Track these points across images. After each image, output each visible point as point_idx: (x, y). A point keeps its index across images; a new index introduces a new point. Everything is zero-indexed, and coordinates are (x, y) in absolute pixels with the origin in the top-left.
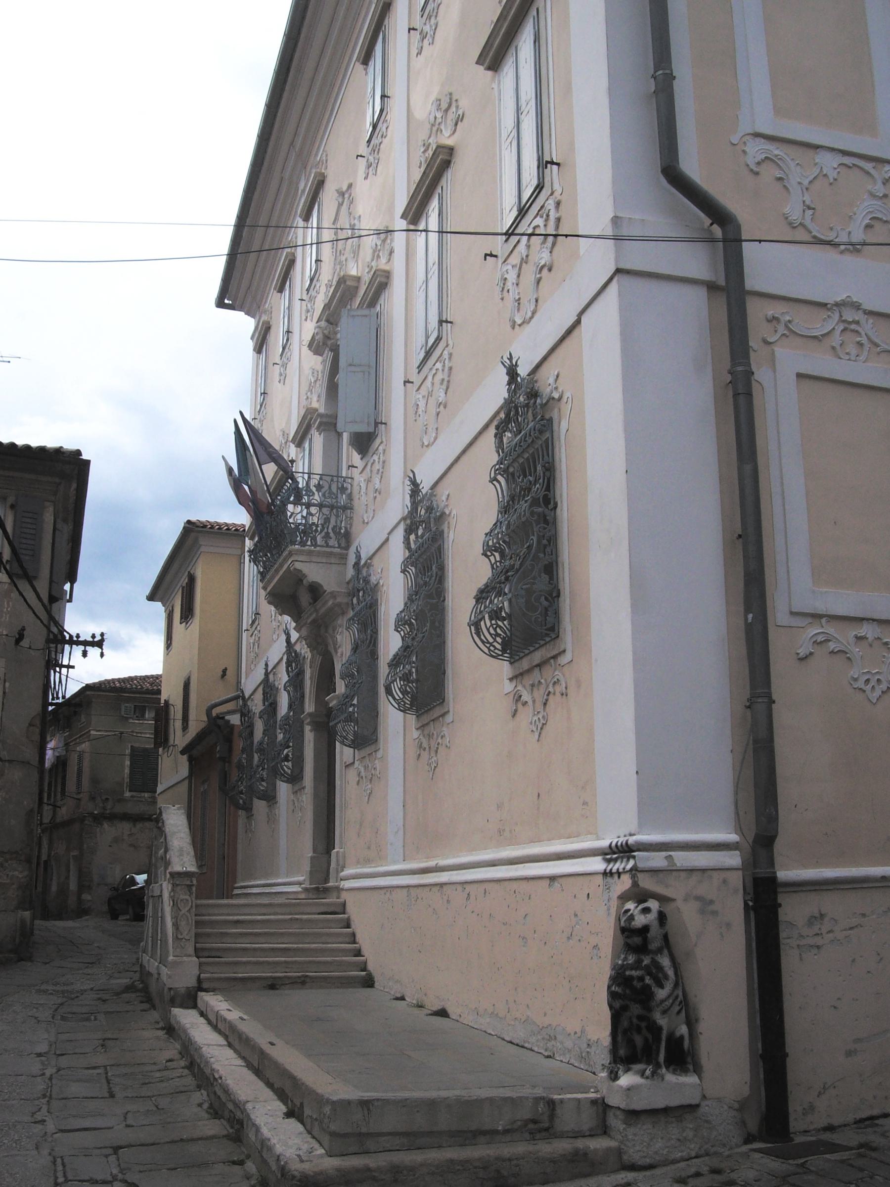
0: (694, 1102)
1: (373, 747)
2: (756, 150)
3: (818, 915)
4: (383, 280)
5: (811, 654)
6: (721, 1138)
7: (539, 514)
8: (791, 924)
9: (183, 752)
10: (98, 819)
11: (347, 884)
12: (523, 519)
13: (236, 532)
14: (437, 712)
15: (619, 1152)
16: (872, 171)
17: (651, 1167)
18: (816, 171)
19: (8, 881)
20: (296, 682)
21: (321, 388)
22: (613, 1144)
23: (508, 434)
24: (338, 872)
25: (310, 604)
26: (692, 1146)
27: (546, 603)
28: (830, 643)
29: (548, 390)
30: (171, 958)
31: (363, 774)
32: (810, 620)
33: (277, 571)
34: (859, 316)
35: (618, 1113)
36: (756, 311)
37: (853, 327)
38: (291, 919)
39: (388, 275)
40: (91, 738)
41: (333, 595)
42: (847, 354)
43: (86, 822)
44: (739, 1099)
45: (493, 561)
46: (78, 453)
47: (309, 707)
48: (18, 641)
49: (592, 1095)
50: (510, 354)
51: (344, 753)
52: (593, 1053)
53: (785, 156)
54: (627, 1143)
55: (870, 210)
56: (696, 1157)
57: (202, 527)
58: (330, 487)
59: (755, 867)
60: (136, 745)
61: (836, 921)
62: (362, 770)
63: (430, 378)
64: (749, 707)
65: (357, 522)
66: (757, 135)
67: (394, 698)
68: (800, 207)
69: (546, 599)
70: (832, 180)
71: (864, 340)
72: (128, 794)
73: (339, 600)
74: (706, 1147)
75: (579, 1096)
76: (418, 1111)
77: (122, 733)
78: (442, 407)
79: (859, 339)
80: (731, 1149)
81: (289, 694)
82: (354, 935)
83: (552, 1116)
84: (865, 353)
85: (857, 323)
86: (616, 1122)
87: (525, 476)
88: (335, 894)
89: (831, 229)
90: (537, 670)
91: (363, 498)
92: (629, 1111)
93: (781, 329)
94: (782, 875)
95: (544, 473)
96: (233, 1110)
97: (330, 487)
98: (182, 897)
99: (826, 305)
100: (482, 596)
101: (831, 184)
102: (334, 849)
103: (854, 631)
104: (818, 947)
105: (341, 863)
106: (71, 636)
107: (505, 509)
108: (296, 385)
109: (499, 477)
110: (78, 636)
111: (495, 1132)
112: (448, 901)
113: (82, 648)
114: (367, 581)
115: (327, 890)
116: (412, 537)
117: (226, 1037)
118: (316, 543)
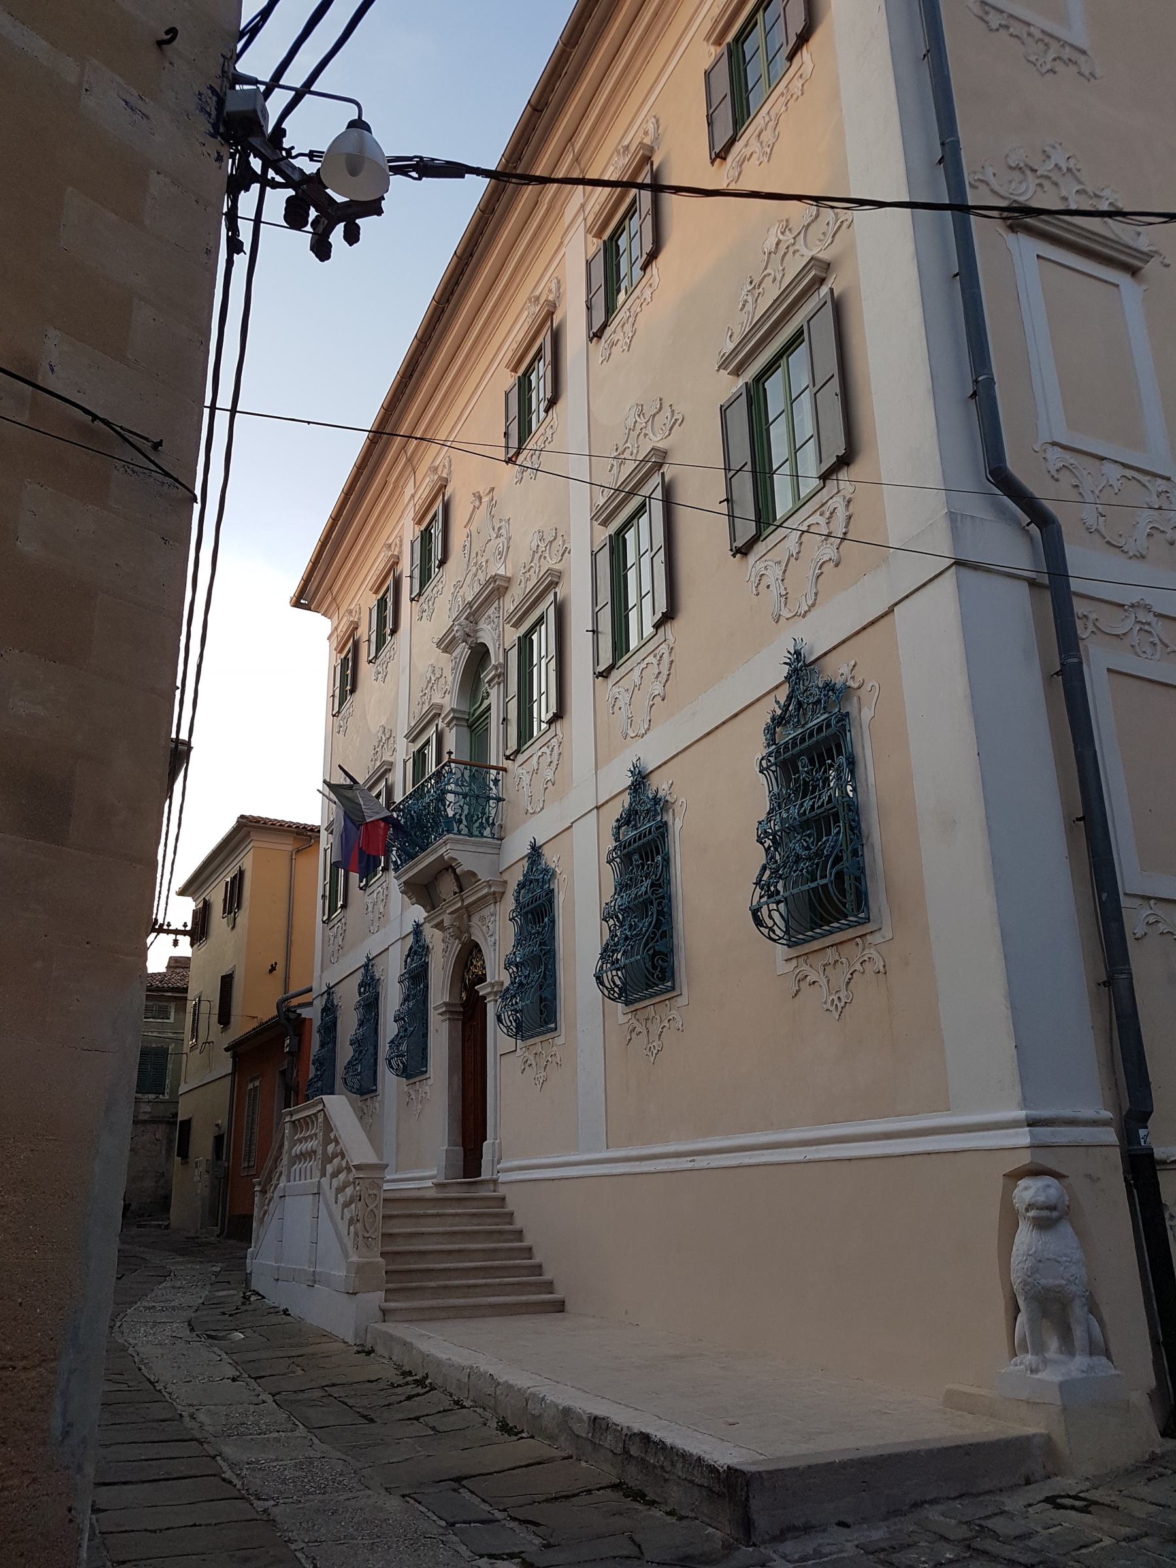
9: (227, 1050)
13: (289, 829)
16: (1147, 484)
20: (417, 977)
25: (455, 893)
28: (1160, 925)
34: (1150, 618)
37: (1146, 627)
41: (489, 884)
42: (1144, 652)
51: (498, 1039)
57: (256, 822)
59: (1130, 1143)
62: (532, 1057)
66: (1054, 444)
70: (1117, 491)
71: (1157, 641)
79: (1152, 639)
84: (1158, 653)
85: (1149, 624)
89: (1121, 536)
93: (1091, 628)
94: (1159, 1153)
99: (1124, 606)
101: (1116, 494)
102: (486, 1140)
110: (169, 925)
113: (172, 937)
118: (471, 834)
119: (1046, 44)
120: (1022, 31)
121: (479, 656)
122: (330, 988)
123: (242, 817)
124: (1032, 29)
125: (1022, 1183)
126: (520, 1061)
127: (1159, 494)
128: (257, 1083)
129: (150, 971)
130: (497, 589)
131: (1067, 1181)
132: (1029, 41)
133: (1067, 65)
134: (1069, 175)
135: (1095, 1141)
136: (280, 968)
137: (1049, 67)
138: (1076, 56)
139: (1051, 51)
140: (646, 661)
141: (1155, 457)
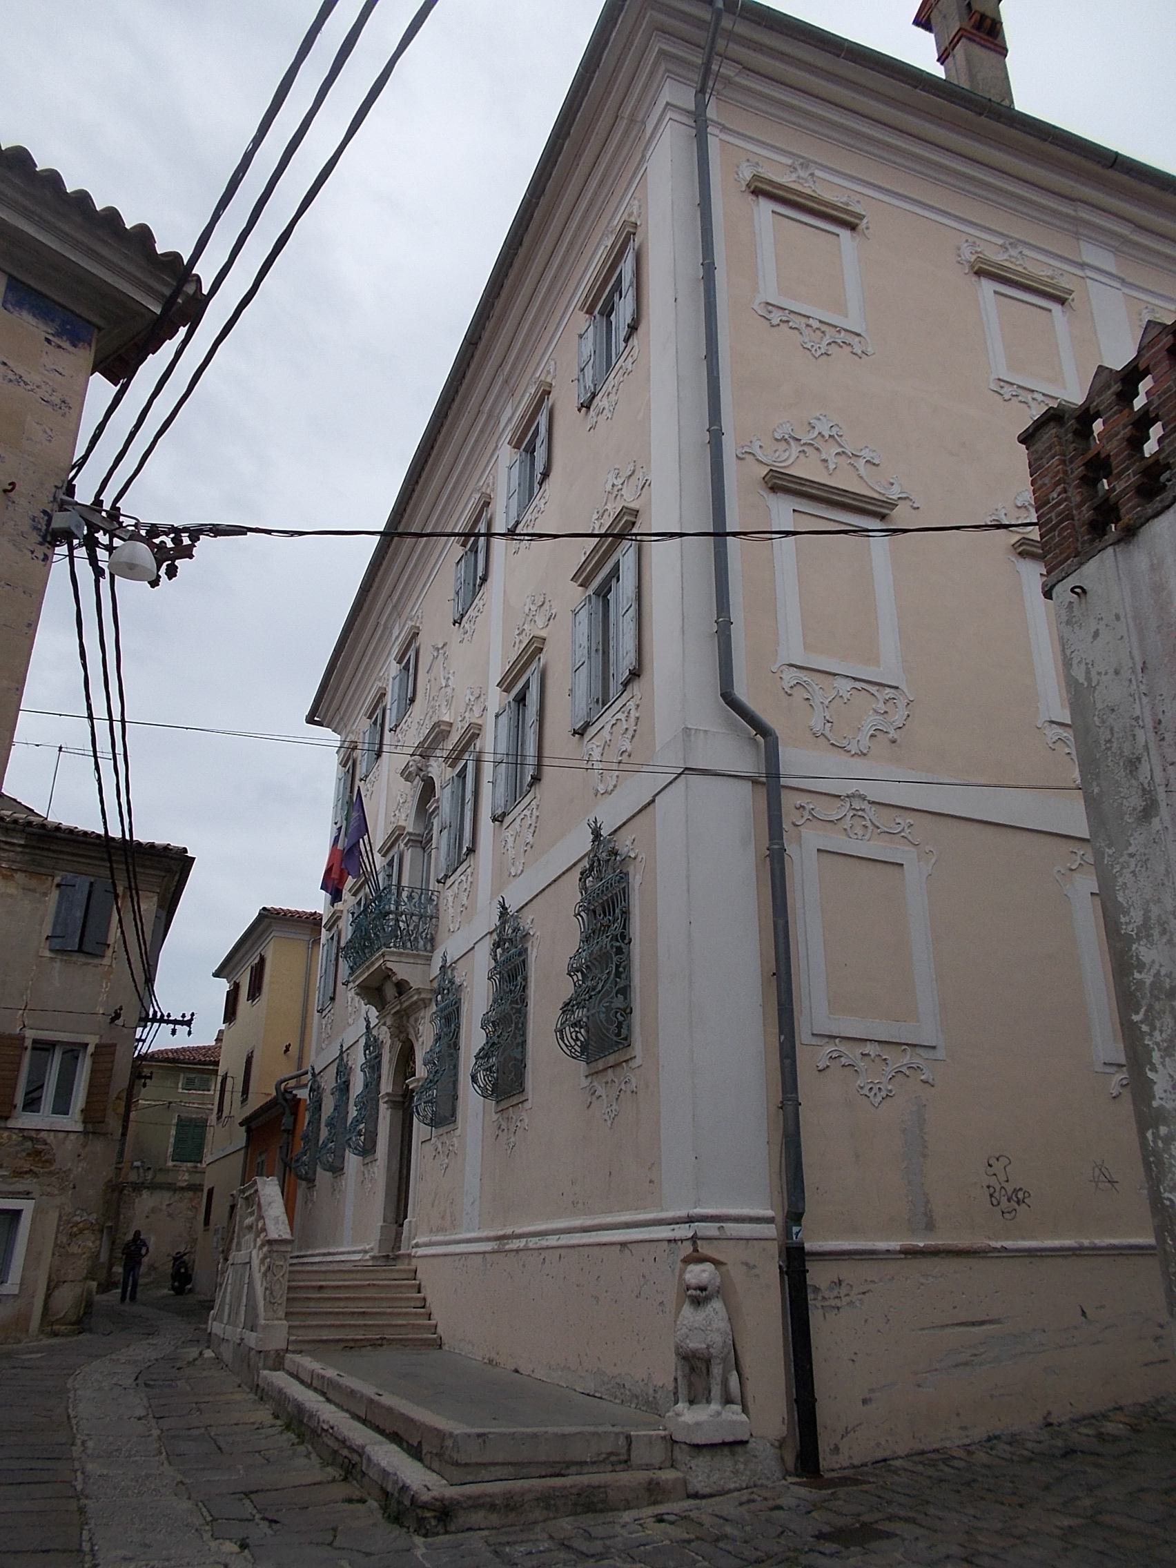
0: (745, 1438)
1: (452, 1126)
2: (790, 676)
3: (837, 1281)
5: (828, 1067)
7: (617, 947)
8: (816, 1290)
9: (241, 1124)
10: (138, 1187)
11: (420, 1251)
12: (604, 950)
14: (514, 1100)
15: (685, 1483)
16: (876, 693)
17: (711, 1496)
18: (834, 693)
19: (80, 1251)
20: (373, 1066)
21: (411, 807)
22: (680, 1475)
23: (591, 878)
24: (409, 1240)
27: (621, 1019)
29: (626, 849)
30: (263, 1322)
31: (440, 1149)
32: (826, 1040)
33: (368, 968)
34: (865, 805)
35: (683, 1446)
36: (789, 801)
37: (860, 813)
38: (369, 1285)
39: (480, 727)
40: (139, 1107)
41: (418, 991)
43: (125, 1192)
44: (779, 1438)
45: (576, 979)
46: (185, 850)
47: (386, 1087)
48: (113, 1020)
49: (662, 1433)
51: (420, 1130)
58: (420, 898)
60: (184, 1115)
61: (851, 1286)
62: (440, 1146)
63: (518, 820)
64: (781, 1108)
65: (442, 929)
67: (479, 1087)
68: (823, 721)
69: (621, 1015)
71: (868, 824)
72: (170, 1164)
73: (423, 996)
75: (652, 1433)
77: (170, 1103)
78: (529, 846)
81: (365, 1075)
82: (425, 1299)
85: (863, 810)
86: (681, 1455)
87: (605, 916)
88: (406, 1261)
90: (610, 1071)
91: (451, 911)
93: (807, 816)
94: (808, 1246)
96: (350, 1456)
97: (420, 898)
98: (277, 1263)
100: (567, 1008)
103: (859, 1049)
104: (838, 1308)
105: (413, 1231)
106: (162, 1015)
107: (586, 939)
108: (383, 802)
109: (582, 913)
110: (169, 1015)
111: (583, 1463)
112: (524, 1266)
113: (171, 1026)
114: (452, 982)
115: (397, 1258)
116: (499, 951)
117: (323, 1394)
119: (823, 332)
121: (428, 789)
123: (264, 909)
125: (691, 1267)
126: (432, 1148)
127: (886, 702)
128: (263, 1157)
130: (439, 732)
131: (723, 1268)
132: (806, 331)
133: (841, 347)
134: (831, 440)
135: (755, 1235)
136: (294, 1050)
137: (823, 351)
138: (849, 338)
139: (828, 337)
140: (616, 717)
141: (888, 668)
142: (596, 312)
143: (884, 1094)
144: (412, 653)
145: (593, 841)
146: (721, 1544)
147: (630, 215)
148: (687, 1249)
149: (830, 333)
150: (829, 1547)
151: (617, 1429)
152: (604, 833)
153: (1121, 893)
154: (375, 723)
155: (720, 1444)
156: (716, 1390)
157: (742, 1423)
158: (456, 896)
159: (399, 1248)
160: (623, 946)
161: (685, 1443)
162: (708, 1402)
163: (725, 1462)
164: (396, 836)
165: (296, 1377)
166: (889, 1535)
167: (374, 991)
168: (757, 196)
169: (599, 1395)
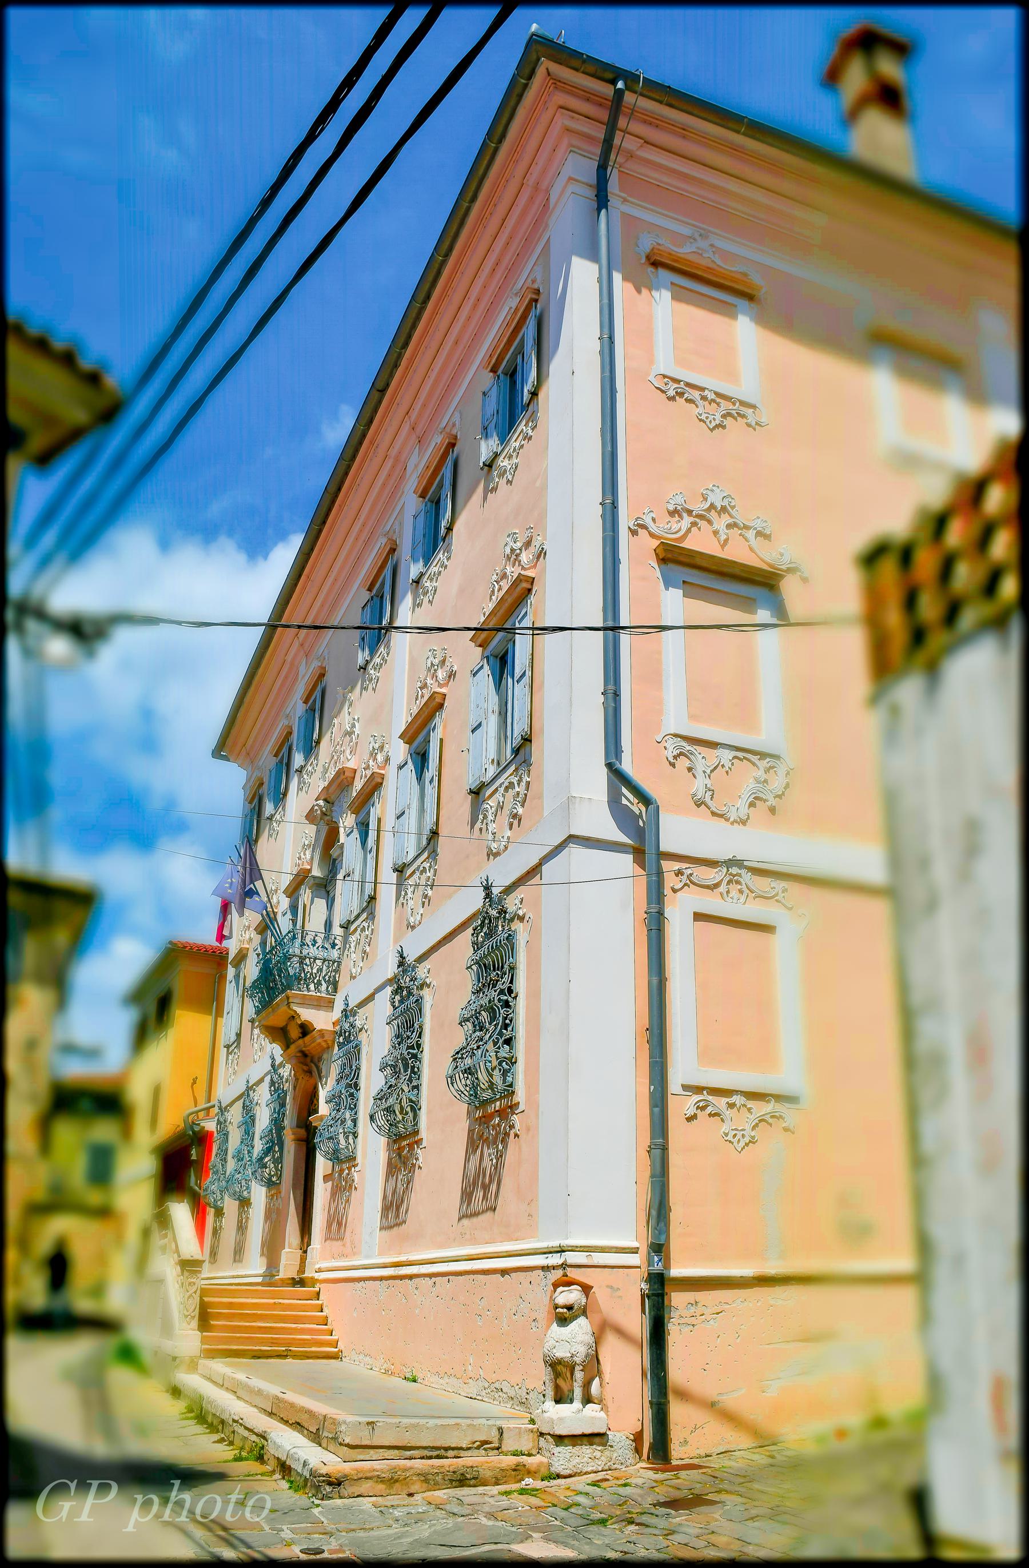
0: (602, 1431)
4: (380, 780)
6: (620, 1458)
16: (757, 762)
17: (570, 1476)
22: (545, 1460)
23: (482, 934)
26: (600, 1463)
39: (382, 777)
41: (322, 1033)
50: (487, 876)
52: (530, 1399)
53: (695, 751)
54: (554, 1459)
55: (754, 791)
56: (602, 1471)
74: (609, 1464)
76: (407, 1431)
80: (627, 1467)
83: (501, 1439)
92: (557, 1436)
95: (509, 971)
100: (458, 1056)
103: (724, 1101)
120: (696, 395)
122: (249, 1089)
123: (171, 943)
124: (706, 392)
129: (758, 610)
130: (342, 780)
132: (701, 403)
133: (736, 419)
139: (722, 408)
142: (500, 372)
143: (747, 1139)
144: (319, 689)
145: (485, 899)
146: (572, 1510)
147: (533, 281)
148: (559, 1273)
149: (725, 405)
150: (663, 1510)
151: (490, 1423)
152: (496, 891)
153: (279, 1060)
154: (281, 761)
155: (580, 1435)
156: (578, 1392)
157: (600, 1419)
158: (358, 943)
159: (304, 1272)
160: (510, 999)
161: (549, 1434)
162: (571, 1401)
163: (586, 1451)
164: (301, 879)
165: (210, 1379)
166: (713, 1503)
167: (280, 1034)
168: (657, 268)
169: (480, 1398)
